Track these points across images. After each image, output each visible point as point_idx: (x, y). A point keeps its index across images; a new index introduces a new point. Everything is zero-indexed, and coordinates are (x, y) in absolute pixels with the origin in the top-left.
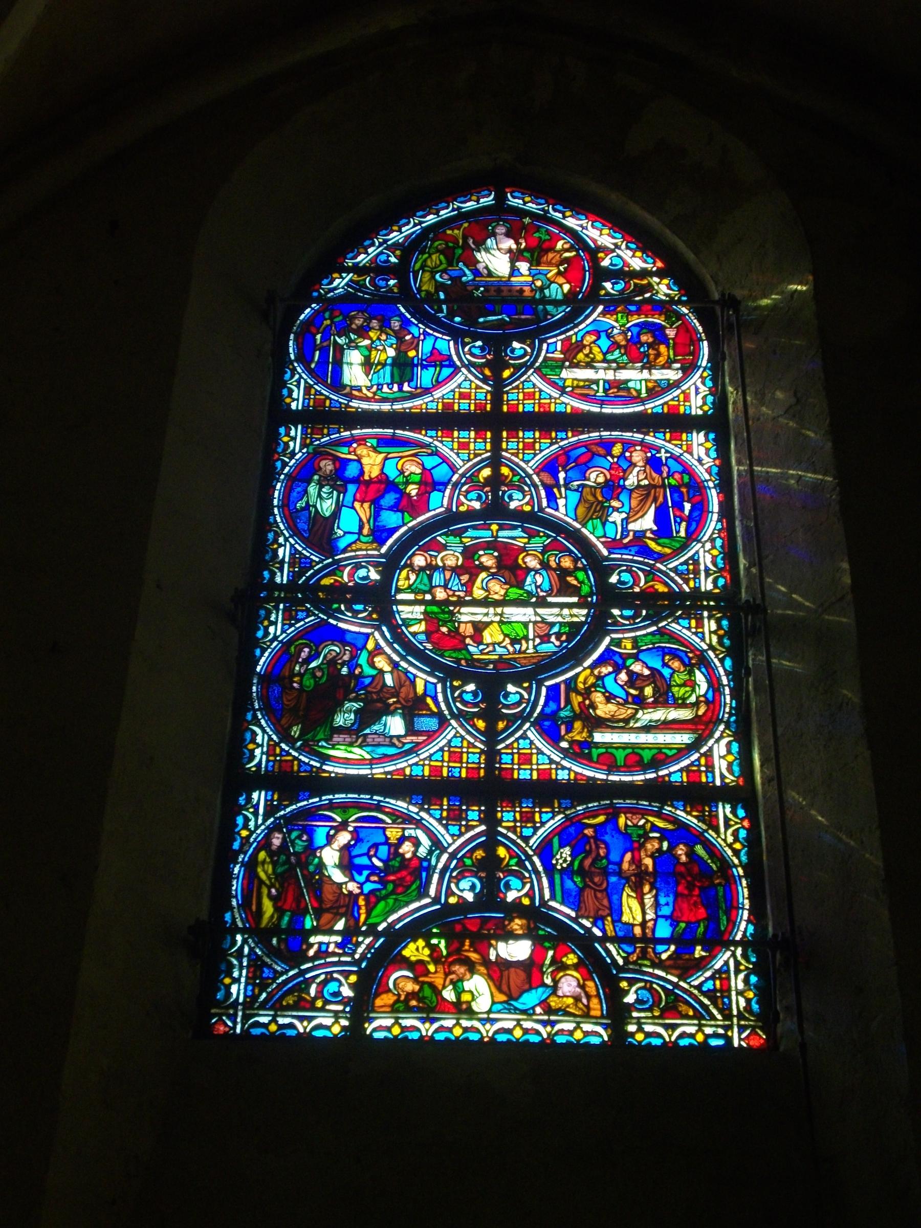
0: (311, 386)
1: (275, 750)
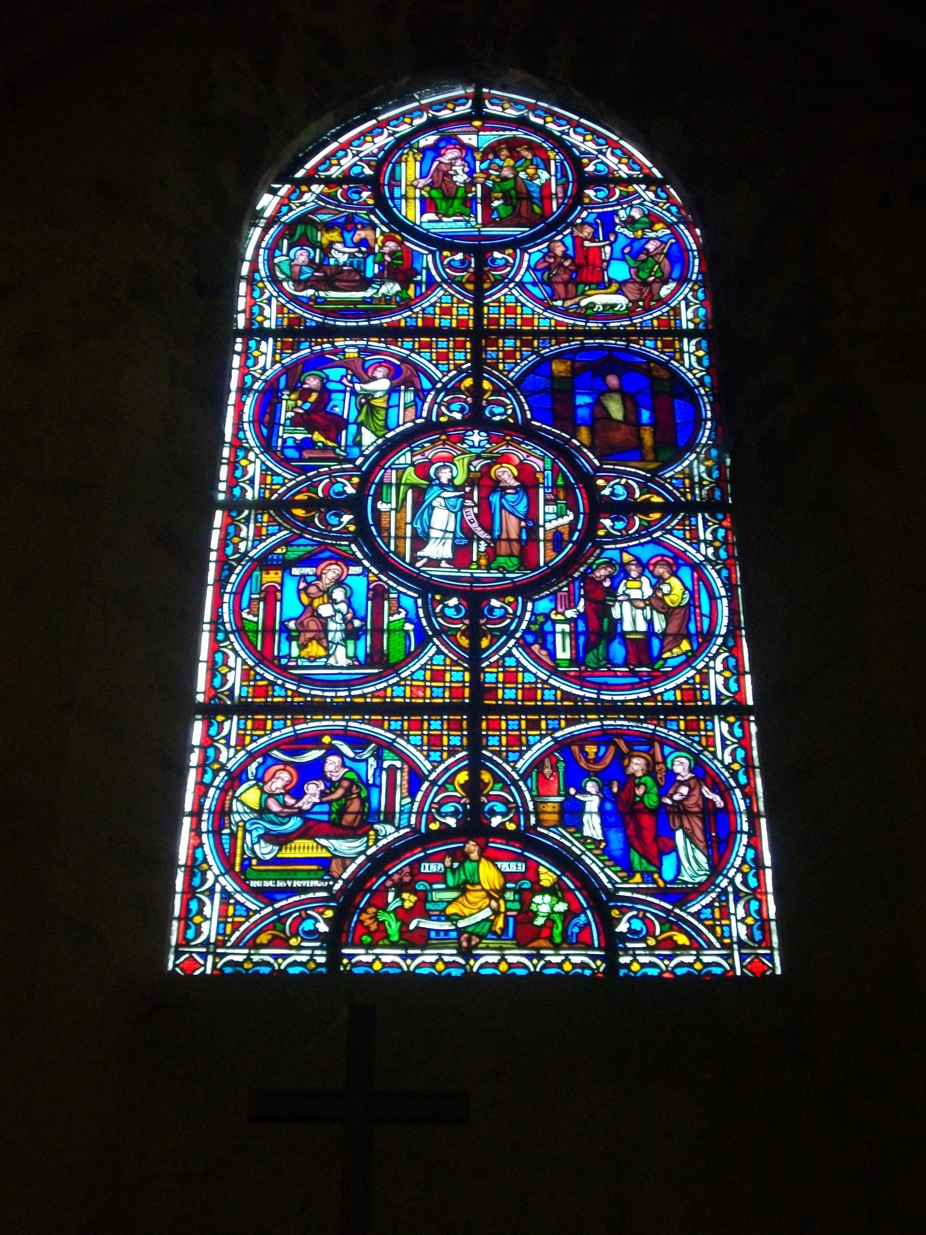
0: (284, 305)
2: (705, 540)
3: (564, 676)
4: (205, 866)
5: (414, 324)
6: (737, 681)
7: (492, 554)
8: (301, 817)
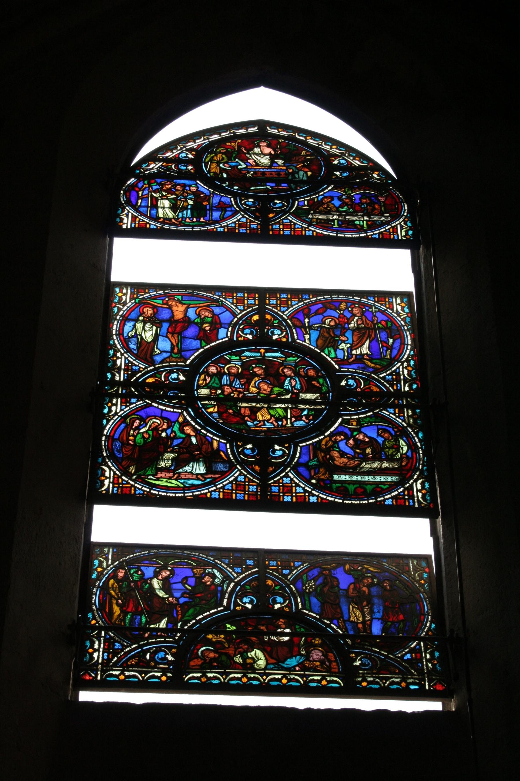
0: (136, 217)
1: (118, 480)
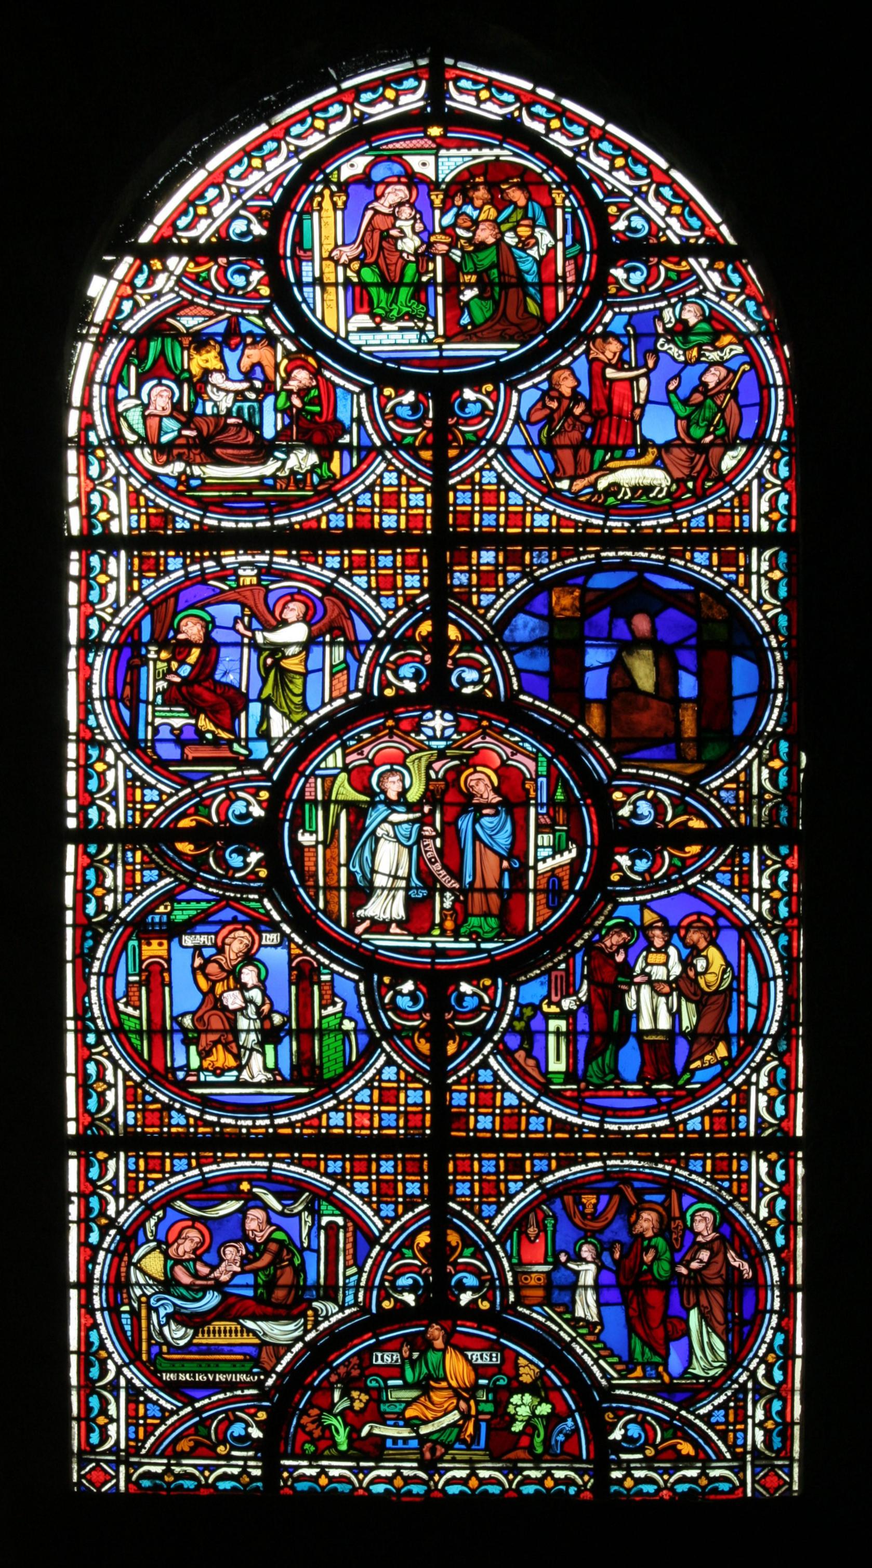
2: (762, 888)
3: (557, 1097)
4: (103, 1354)
5: (341, 524)
6: (785, 1102)
7: (461, 913)
8: (220, 1292)
